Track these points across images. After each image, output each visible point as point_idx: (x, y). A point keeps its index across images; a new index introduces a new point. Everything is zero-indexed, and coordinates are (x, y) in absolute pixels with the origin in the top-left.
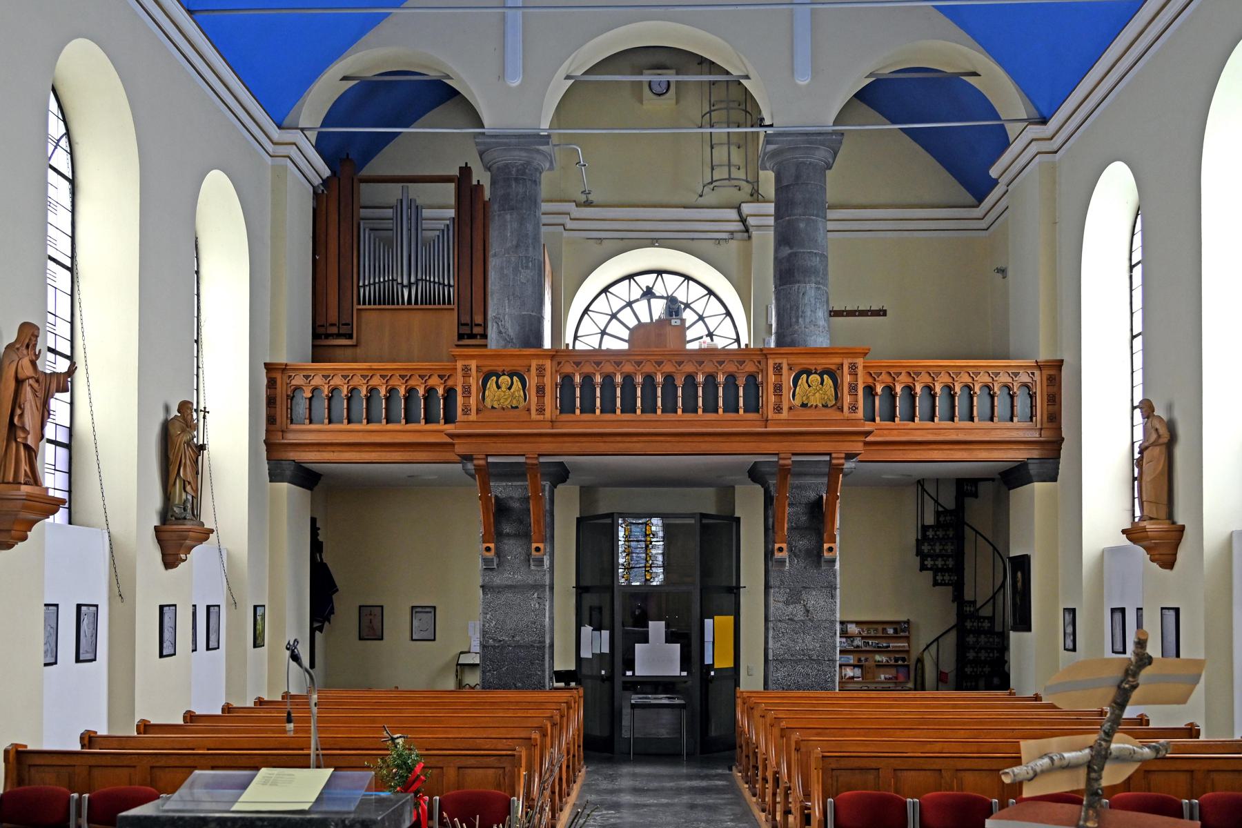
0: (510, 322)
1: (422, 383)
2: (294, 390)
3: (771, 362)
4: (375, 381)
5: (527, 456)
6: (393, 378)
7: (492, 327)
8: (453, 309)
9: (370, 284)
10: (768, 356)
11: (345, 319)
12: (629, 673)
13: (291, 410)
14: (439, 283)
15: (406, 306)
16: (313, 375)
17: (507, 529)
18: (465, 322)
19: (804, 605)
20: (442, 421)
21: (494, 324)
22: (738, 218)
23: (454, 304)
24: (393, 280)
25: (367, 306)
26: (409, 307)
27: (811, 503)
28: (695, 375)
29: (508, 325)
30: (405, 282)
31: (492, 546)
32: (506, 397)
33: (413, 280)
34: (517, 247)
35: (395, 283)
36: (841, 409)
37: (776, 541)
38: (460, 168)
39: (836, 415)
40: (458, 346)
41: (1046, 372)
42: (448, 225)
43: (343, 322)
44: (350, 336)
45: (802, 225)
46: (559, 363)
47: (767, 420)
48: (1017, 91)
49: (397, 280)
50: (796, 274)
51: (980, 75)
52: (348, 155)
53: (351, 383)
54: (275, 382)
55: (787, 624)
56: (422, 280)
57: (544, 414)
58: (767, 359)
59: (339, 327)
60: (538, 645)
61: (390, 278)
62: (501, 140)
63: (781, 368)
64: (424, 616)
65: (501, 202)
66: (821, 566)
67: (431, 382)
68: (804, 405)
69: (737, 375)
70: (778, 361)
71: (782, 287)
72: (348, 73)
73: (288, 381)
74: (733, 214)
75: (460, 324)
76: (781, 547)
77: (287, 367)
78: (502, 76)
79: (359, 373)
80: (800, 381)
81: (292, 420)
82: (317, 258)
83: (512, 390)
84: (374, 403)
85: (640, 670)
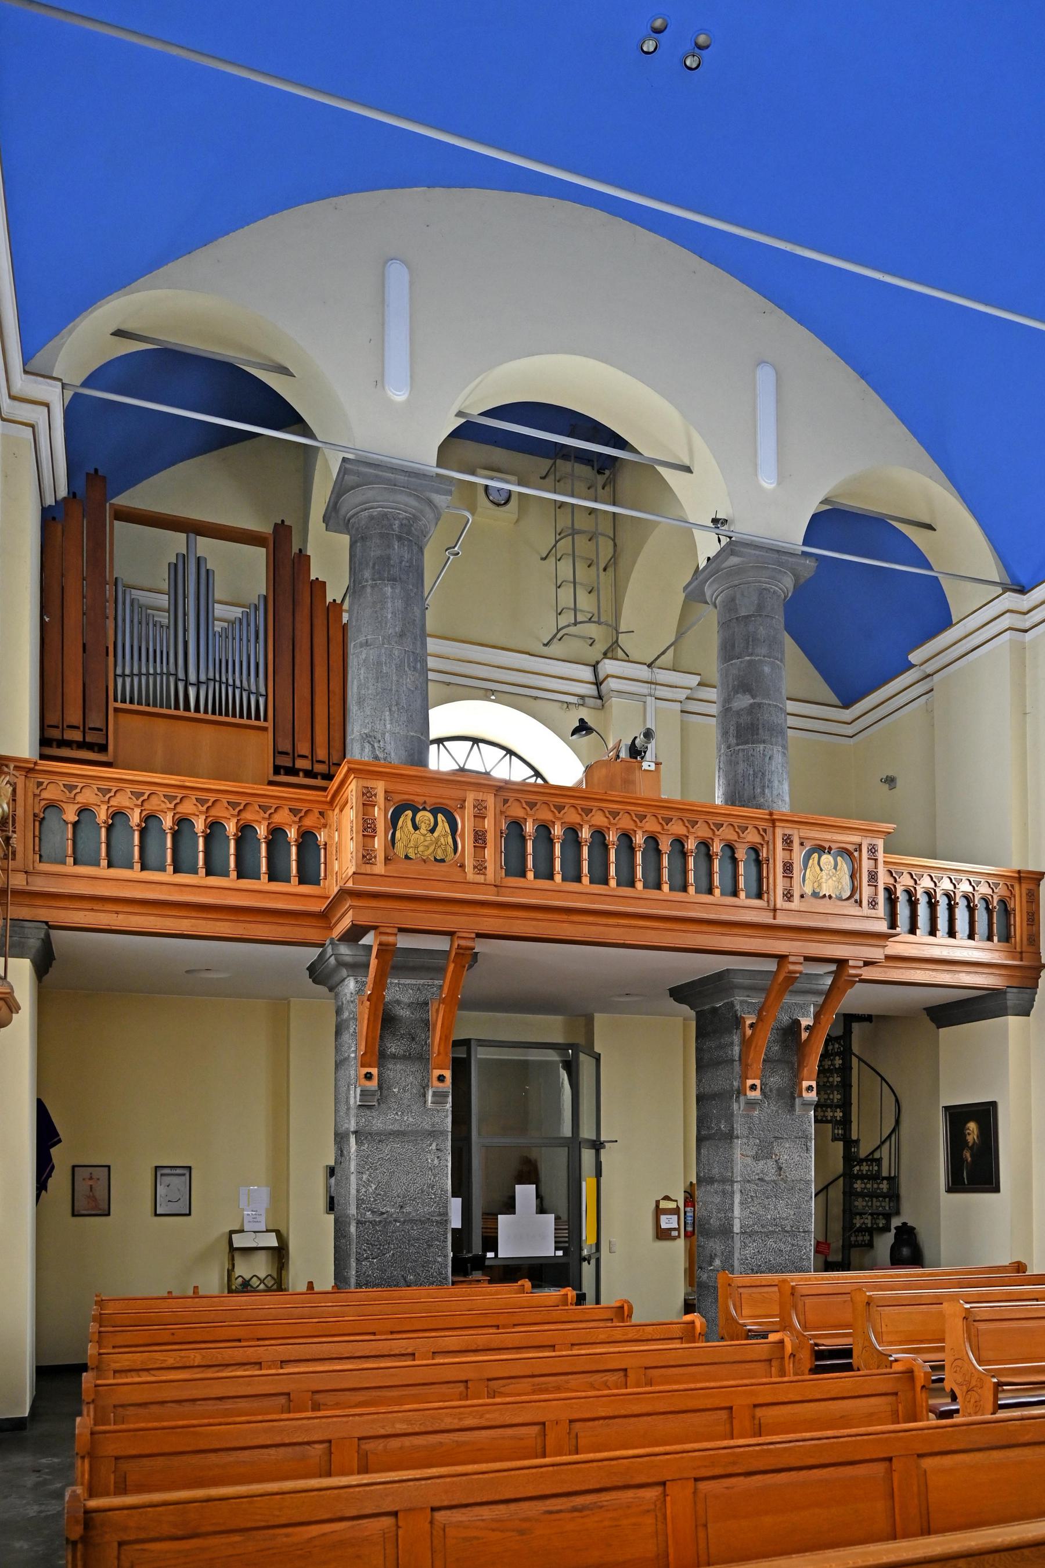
0: (392, 743)
2: (47, 807)
3: (779, 833)
4: (187, 808)
6: (218, 805)
8: (265, 729)
10: (777, 824)
11: (95, 721)
12: (490, 1255)
14: (242, 688)
15: (192, 714)
16: (81, 785)
17: (393, 1048)
18: (284, 750)
19: (776, 1161)
21: (367, 745)
22: (592, 678)
23: (266, 720)
26: (197, 715)
27: (783, 1029)
28: (685, 838)
29: (390, 748)
31: (374, 1071)
32: (426, 843)
36: (859, 903)
37: (749, 1076)
39: (855, 910)
40: (271, 783)
41: (1025, 886)
44: (103, 748)
45: (767, 669)
46: (506, 801)
47: (775, 910)
48: (991, 551)
49: (176, 675)
50: (760, 731)
51: (935, 530)
53: (146, 806)
55: (757, 1185)
56: (214, 680)
57: (485, 874)
58: (774, 827)
60: (438, 1218)
61: (165, 670)
62: (384, 474)
63: (792, 842)
64: (175, 1181)
66: (795, 1111)
68: (815, 895)
69: (737, 845)
70: (788, 832)
71: (740, 747)
74: (587, 673)
75: (277, 753)
76: (754, 1085)
77: (37, 768)
78: (379, 383)
80: (811, 861)
81: (41, 856)
82: (47, 620)
83: (436, 834)
85: (505, 1250)
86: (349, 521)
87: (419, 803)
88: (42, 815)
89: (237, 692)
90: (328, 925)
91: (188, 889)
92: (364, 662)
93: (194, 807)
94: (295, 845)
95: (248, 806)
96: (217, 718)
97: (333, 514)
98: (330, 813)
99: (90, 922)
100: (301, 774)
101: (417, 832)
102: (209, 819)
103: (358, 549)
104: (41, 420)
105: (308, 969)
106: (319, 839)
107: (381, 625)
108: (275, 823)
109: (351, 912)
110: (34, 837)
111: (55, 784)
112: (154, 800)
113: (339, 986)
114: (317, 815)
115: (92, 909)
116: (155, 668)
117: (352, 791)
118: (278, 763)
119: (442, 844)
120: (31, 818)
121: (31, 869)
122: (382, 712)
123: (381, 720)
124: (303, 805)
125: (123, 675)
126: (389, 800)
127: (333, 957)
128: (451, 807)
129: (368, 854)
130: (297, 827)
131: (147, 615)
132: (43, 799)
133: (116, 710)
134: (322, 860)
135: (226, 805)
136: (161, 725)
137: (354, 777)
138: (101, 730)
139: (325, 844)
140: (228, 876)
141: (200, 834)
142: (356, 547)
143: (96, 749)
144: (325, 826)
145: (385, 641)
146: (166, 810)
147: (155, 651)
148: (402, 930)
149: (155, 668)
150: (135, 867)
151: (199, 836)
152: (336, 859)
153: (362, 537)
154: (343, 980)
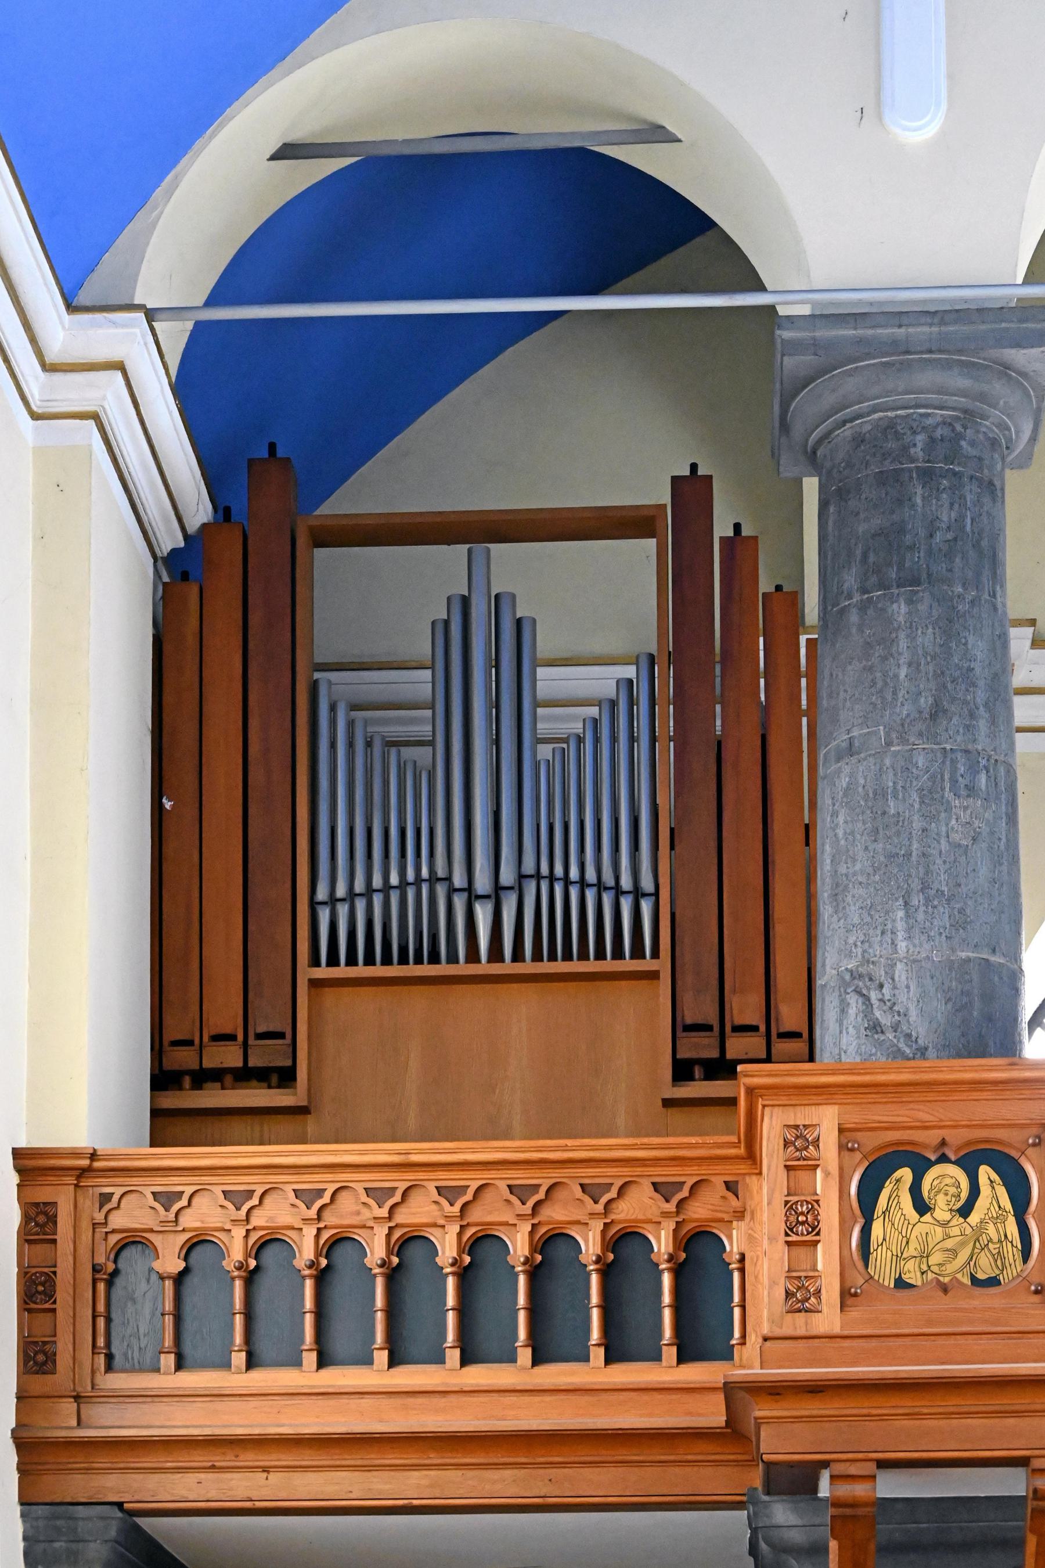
1: (593, 1215)
2: (121, 1248)
5: (839, 1469)
6: (488, 1196)
7: (843, 1011)
8: (653, 976)
9: (352, 895)
13: (109, 1320)
15: (484, 967)
16: (189, 1190)
20: (670, 1354)
21: (853, 1000)
23: (655, 954)
24: (433, 879)
25: (342, 971)
26: (496, 969)
29: (908, 1000)
30: (483, 883)
32: (949, 1244)
33: (507, 877)
34: (934, 716)
35: (441, 890)
38: (675, 480)
43: (261, 1029)
44: (286, 1077)
49: (449, 879)
52: (272, 447)
53: (330, 1218)
54: (53, 1220)
56: (538, 876)
59: (245, 1045)
61: (425, 873)
65: (872, 558)
67: (626, 1211)
72: (297, 135)
73: (100, 1217)
75: (680, 1028)
77: (97, 1164)
79: (359, 1181)
81: (110, 1357)
82: (168, 805)
83: (974, 1218)
84: (414, 1285)
86: (814, 453)
87: (925, 1146)
88: (111, 1266)
91: (420, 1400)
92: (845, 795)
93: (434, 1207)
94: (668, 1269)
96: (546, 967)
97: (783, 440)
98: (752, 1181)
99: (210, 1496)
101: (927, 1217)
104: (109, 397)
107: (883, 698)
108: (620, 1222)
110: (94, 1317)
112: (345, 1201)
114: (722, 1190)
115: (213, 1467)
119: (990, 1241)
120: (87, 1275)
121: (86, 1389)
122: (887, 913)
123: (883, 933)
124: (688, 1170)
126: (852, 1150)
128: (1010, 1146)
130: (673, 1226)
132: (114, 1231)
134: (736, 1298)
136: (419, 999)
141: (448, 1270)
143: (274, 1079)
145: (894, 735)
146: (371, 1224)
148: (883, 1464)
150: (304, 1362)
151: (447, 1274)
153: (839, 490)
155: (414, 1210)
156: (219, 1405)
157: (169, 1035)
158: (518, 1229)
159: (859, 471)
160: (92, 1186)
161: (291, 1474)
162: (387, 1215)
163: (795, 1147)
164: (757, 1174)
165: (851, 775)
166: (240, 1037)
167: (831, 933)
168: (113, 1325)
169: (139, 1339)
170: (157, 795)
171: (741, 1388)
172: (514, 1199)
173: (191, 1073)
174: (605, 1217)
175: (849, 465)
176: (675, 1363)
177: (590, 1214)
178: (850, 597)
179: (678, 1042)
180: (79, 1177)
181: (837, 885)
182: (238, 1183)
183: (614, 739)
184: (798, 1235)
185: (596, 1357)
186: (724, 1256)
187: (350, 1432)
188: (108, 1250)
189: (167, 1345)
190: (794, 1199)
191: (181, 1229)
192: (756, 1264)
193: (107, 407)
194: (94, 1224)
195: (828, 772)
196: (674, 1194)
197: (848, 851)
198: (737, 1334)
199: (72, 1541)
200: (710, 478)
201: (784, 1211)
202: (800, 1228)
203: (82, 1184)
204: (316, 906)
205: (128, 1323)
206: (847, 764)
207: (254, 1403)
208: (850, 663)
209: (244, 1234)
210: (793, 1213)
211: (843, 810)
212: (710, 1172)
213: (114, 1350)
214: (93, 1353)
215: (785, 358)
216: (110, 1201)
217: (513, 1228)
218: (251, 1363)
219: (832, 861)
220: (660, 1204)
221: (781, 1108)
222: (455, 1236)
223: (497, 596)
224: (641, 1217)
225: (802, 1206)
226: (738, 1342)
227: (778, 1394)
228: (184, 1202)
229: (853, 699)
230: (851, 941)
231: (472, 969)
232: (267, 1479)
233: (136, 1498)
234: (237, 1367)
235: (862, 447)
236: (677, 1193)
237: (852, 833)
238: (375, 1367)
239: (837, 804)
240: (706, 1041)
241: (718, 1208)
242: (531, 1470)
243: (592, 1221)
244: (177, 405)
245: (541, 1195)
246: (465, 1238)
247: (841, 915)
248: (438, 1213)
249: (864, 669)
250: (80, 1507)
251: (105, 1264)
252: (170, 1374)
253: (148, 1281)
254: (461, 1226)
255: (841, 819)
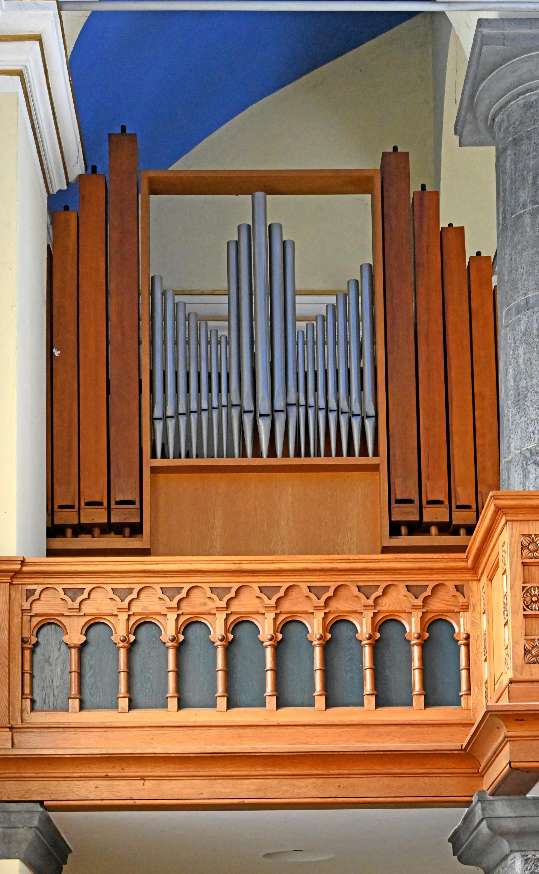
1: (366, 607)
6: (294, 593)
8: (375, 468)
9: (177, 414)
13: (32, 677)
15: (265, 460)
16: (88, 588)
23: (376, 453)
25: (171, 462)
26: (272, 461)
30: (264, 407)
33: (279, 404)
38: (384, 154)
40: (385, 550)
42: (334, 306)
43: (119, 498)
49: (240, 405)
52: (123, 128)
53: (186, 608)
56: (298, 405)
77: (25, 569)
81: (33, 701)
82: (56, 353)
88: (34, 640)
89: (332, 417)
90: (476, 771)
92: (524, 335)
93: (258, 600)
94: (418, 644)
95: (243, 591)
96: (303, 461)
98: (474, 585)
99: (104, 796)
100: (434, 530)
102: (281, 618)
103: (509, 159)
105: (450, 840)
106: (457, 630)
108: (384, 612)
109: (507, 748)
110: (23, 673)
111: (51, 590)
113: (500, 868)
114: (453, 591)
115: (107, 776)
116: (210, 401)
117: (503, 546)
118: (396, 518)
120: (18, 645)
121: (18, 723)
124: (431, 577)
125: (165, 418)
127: (484, 823)
129: (533, 647)
130: (420, 615)
131: (209, 332)
132: (36, 615)
133: (154, 470)
134: (463, 664)
135: (306, 591)
137: (507, 521)
138: (133, 503)
139: (468, 637)
140: (313, 705)
141: (268, 643)
142: (506, 157)
143: (127, 531)
144: (466, 607)
146: (214, 611)
147: (209, 376)
149: (210, 401)
151: (266, 646)
152: (485, 660)
153: (515, 140)
154: (505, 858)
155: (242, 603)
156: (110, 734)
157: (58, 502)
158: (315, 616)
159: (529, 126)
160: (22, 584)
161: (160, 781)
162: (226, 606)
163: (529, 549)
164: (477, 580)
165: (528, 322)
166: (105, 504)
167: (514, 427)
168: (35, 680)
169: (53, 690)
170: (49, 348)
171: (496, 715)
172: (312, 596)
173: (72, 526)
174: (375, 609)
175: (522, 123)
176: (423, 708)
177: (364, 606)
178: (524, 207)
179: (392, 510)
180: (12, 578)
181: (519, 394)
182: (122, 583)
183: (346, 319)
184: (532, 610)
185: (369, 703)
186: (455, 635)
187: (203, 752)
188: (32, 628)
189: (73, 693)
190: (528, 585)
191: (83, 614)
192: (477, 640)
193: (28, 67)
194: (22, 610)
195: (510, 321)
196: (421, 593)
197: (527, 371)
198: (464, 687)
199: (8, 828)
200: (407, 154)
201: (522, 594)
202: (534, 605)
203: (14, 583)
204: (154, 421)
205: (46, 678)
206: (525, 315)
207: (134, 732)
208: (525, 250)
209: (127, 618)
210: (529, 595)
211: (523, 346)
212: (444, 579)
213: (36, 697)
214: (22, 698)
215: (485, 48)
216: (34, 594)
217: (311, 616)
218: (132, 706)
219: (515, 379)
220: (411, 600)
221: (519, 522)
222: (272, 620)
223: (270, 226)
224: (398, 608)
225: (535, 590)
226: (466, 693)
227: (523, 720)
228: (85, 596)
229: (528, 272)
230: (530, 430)
231: (257, 462)
232: (144, 785)
233: (52, 798)
234: (122, 708)
235: (531, 111)
236: (423, 592)
237: (530, 360)
238: (218, 709)
239: (518, 342)
240: (410, 509)
241: (450, 603)
242: (326, 779)
243: (366, 611)
244: (70, 81)
245: (331, 593)
246: (278, 622)
247: (522, 414)
248: (259, 605)
249: (536, 253)
250: (13, 804)
251: (30, 638)
252: (76, 713)
253: (59, 650)
254: (276, 614)
255: (521, 351)
